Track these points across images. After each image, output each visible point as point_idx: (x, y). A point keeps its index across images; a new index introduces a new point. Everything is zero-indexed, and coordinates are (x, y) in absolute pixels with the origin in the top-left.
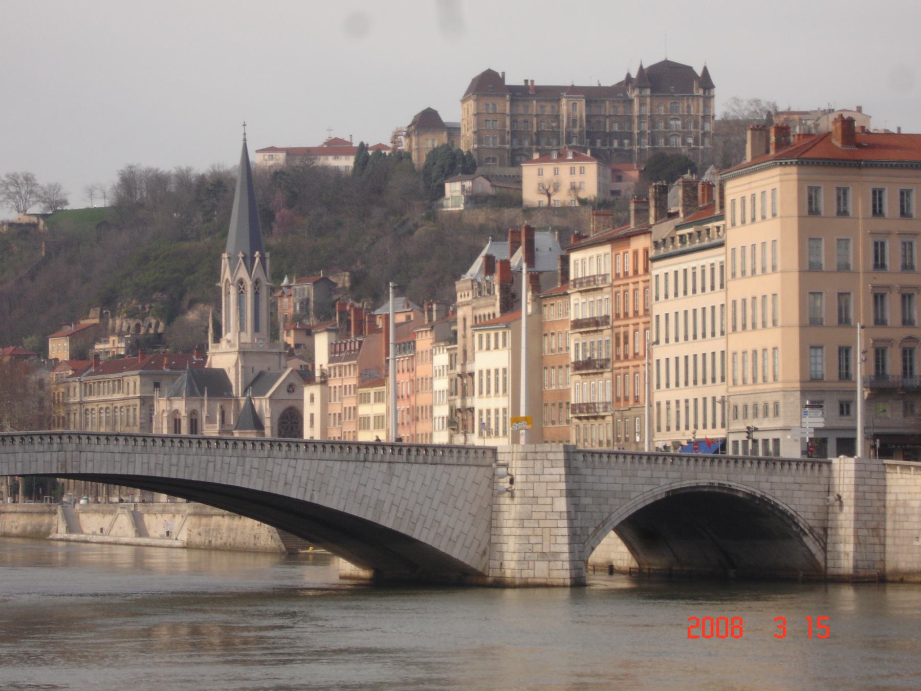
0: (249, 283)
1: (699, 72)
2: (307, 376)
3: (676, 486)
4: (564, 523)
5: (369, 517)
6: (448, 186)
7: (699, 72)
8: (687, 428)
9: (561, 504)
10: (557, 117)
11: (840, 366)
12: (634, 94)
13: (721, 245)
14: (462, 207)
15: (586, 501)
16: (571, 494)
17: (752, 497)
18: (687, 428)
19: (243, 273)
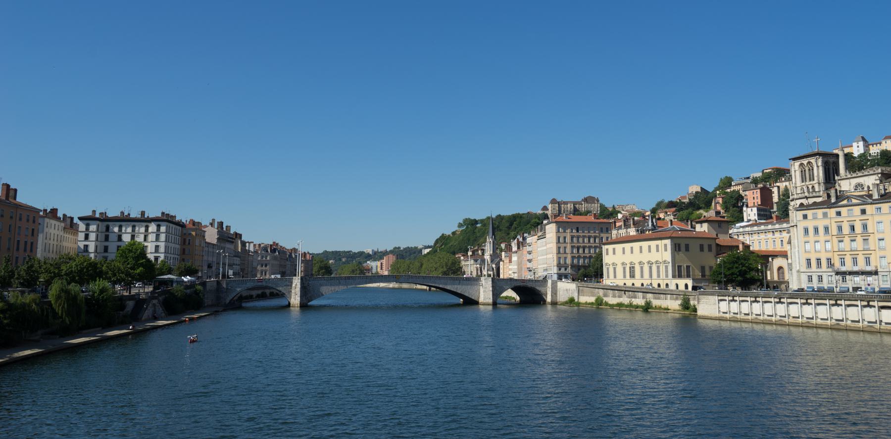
0: (492, 242)
1: (596, 198)
2: (501, 260)
3: (516, 285)
4: (491, 292)
5: (455, 291)
6: (544, 222)
7: (596, 198)
8: (25, 250)
9: (491, 289)
10: (568, 207)
11: (821, 265)
12: (583, 203)
13: (545, 237)
14: (826, 199)
15: (498, 288)
16: (493, 287)
17: (532, 287)
18: (25, 250)
19: (491, 240)
